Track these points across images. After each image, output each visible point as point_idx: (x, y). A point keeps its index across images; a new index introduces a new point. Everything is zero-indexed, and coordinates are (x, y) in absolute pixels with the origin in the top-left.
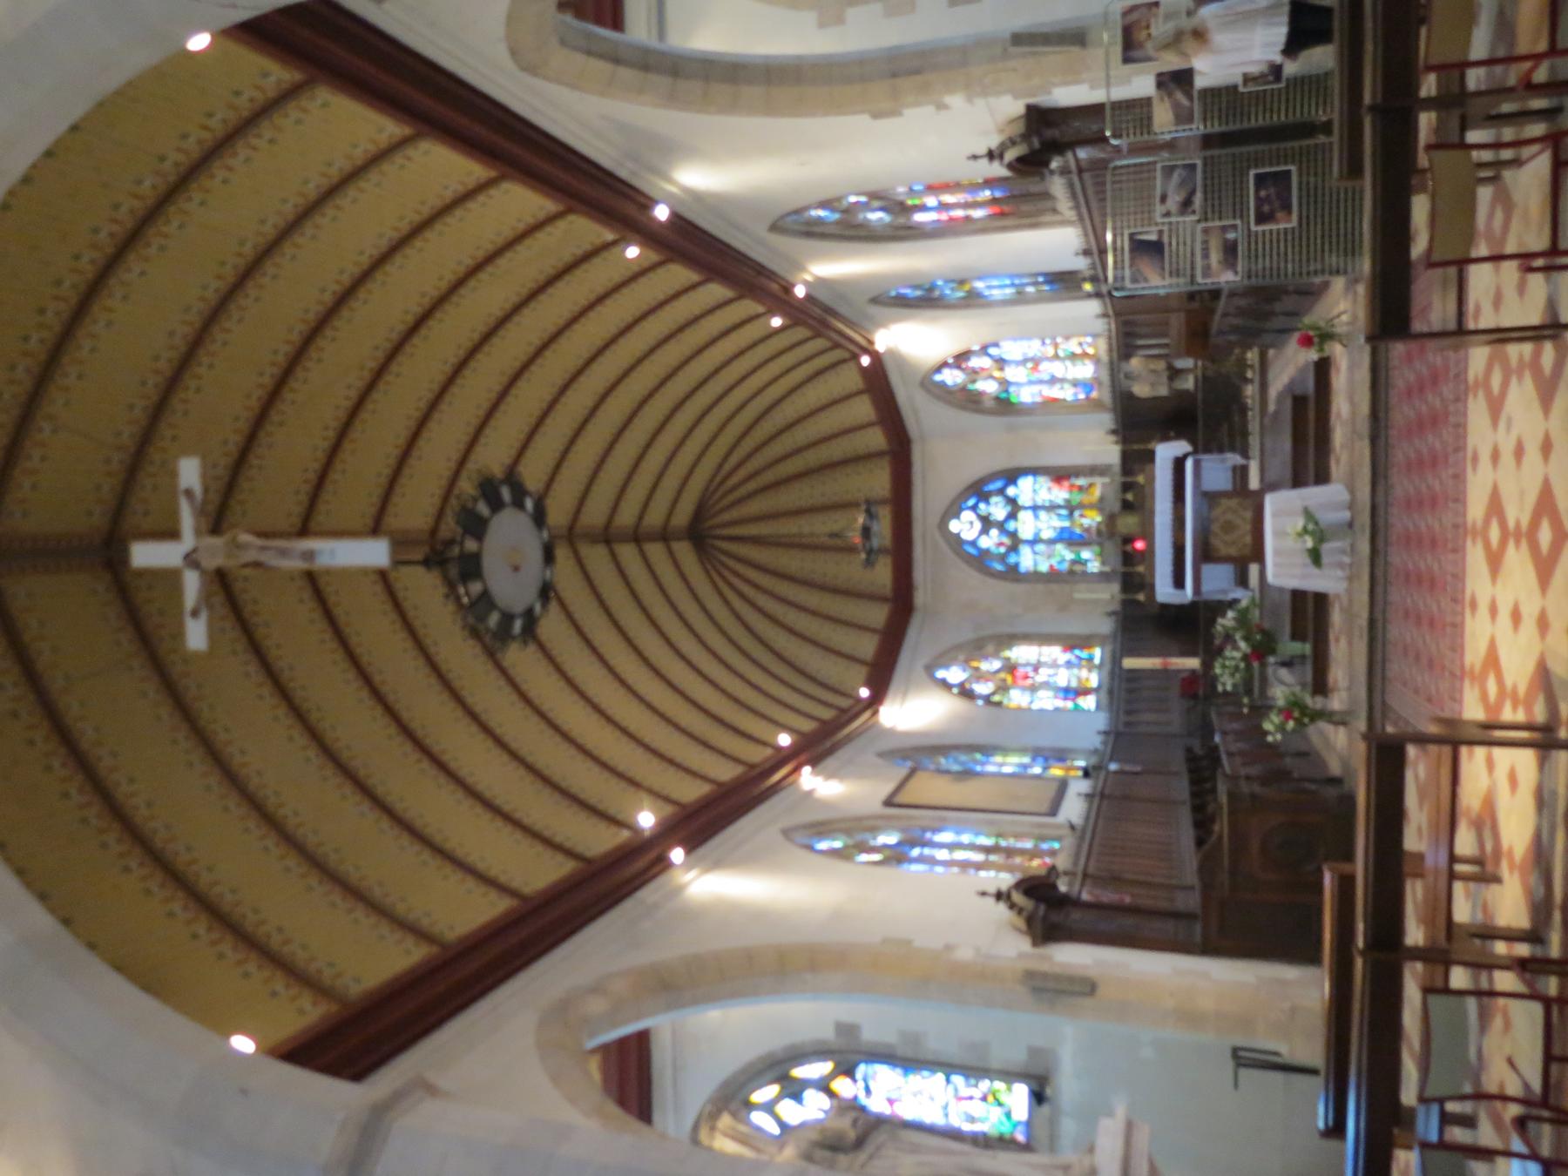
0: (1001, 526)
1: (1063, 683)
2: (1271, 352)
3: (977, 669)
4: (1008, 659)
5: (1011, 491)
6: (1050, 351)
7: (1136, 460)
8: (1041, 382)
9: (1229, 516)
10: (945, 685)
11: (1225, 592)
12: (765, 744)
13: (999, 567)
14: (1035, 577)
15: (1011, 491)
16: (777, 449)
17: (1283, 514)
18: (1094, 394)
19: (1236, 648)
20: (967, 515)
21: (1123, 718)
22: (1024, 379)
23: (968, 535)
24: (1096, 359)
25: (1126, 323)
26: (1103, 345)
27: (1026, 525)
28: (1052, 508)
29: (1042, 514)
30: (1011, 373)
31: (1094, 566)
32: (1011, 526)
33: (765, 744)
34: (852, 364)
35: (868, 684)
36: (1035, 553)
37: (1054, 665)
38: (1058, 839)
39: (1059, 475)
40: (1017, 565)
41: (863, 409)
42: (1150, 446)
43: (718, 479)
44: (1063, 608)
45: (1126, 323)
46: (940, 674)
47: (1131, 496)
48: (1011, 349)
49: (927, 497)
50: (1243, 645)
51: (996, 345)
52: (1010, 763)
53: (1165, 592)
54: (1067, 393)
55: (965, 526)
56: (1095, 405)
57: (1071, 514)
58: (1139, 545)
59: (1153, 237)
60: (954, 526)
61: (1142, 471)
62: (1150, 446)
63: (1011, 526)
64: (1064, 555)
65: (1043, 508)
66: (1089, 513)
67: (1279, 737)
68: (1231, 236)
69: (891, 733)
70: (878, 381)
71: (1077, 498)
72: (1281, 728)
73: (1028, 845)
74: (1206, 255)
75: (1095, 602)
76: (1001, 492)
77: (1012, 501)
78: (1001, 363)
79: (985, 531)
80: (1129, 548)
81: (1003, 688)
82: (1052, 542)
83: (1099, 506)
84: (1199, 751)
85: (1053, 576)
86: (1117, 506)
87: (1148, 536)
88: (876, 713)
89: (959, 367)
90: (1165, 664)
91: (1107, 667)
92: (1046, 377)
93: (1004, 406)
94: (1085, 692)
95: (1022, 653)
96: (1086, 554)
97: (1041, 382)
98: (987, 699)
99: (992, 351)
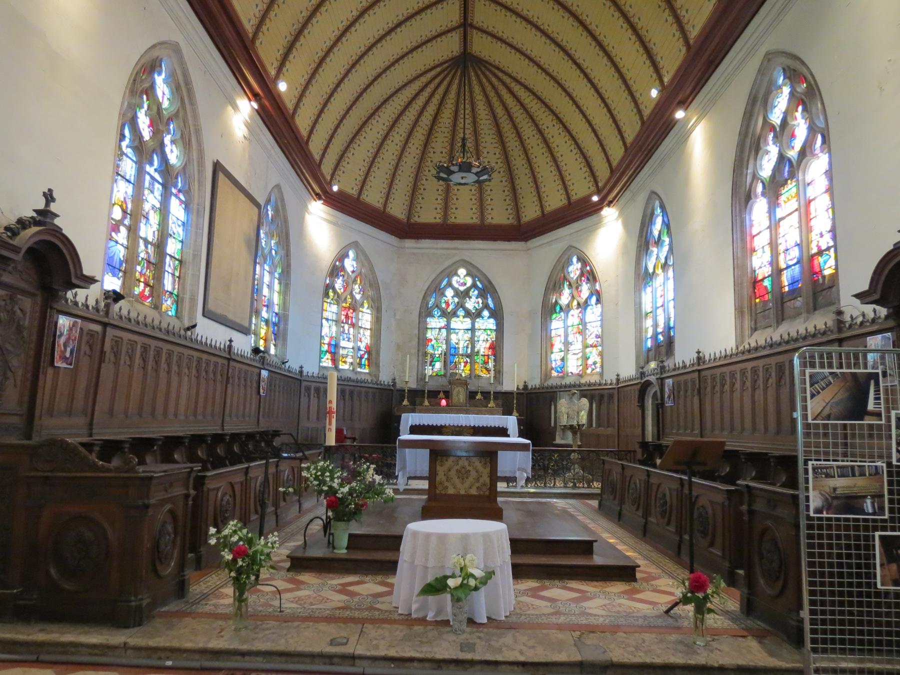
0: (460, 305)
1: (343, 343)
2: (595, 503)
3: (355, 281)
4: (362, 305)
5: (486, 313)
6: (591, 340)
7: (506, 402)
8: (566, 335)
9: (473, 474)
10: (342, 256)
11: (404, 468)
12: (279, 70)
13: (431, 302)
14: (423, 328)
15: (486, 313)
16: (528, 131)
17: (477, 542)
18: (554, 374)
19: (344, 482)
20: (469, 281)
21: (313, 385)
22: (569, 323)
23: (454, 280)
24: (580, 376)
25: (611, 396)
26: (595, 379)
27: (460, 323)
28: (472, 341)
29: (468, 335)
30: (575, 312)
31: (429, 371)
32: (461, 313)
33: (279, 70)
34: (593, 189)
35: (340, 192)
36: (440, 329)
37: (357, 339)
38: (178, 316)
39: (496, 348)
40: (433, 316)
41: (555, 201)
42: (515, 413)
43: (508, 80)
44: (399, 347)
45: (611, 396)
46: (351, 254)
47: (478, 399)
48: (594, 313)
49: (485, 253)
50: (346, 489)
51: (598, 301)
52: (271, 291)
53: (409, 419)
54: (556, 356)
55: (462, 278)
56: (547, 376)
57: (468, 356)
58: (444, 402)
59: (871, 406)
60: (462, 272)
61: (497, 405)
62: (515, 413)
63: (461, 313)
64: (438, 348)
65: (473, 335)
66: (468, 367)
67: (213, 541)
68: (868, 505)
69: (304, 208)
70: (580, 211)
71: (479, 359)
72: (225, 543)
73: (168, 283)
74: (844, 472)
75: (404, 372)
76: (486, 306)
77: (478, 314)
78: (584, 306)
79: (457, 293)
80: (442, 395)
81: (338, 299)
82: (448, 340)
83: (472, 375)
84: (277, 442)
85: (423, 342)
86: (472, 388)
87: (451, 408)
88: (319, 197)
89: (582, 274)
90: (330, 412)
91: (354, 377)
92: (570, 339)
93: (549, 310)
94: (334, 360)
95: (366, 318)
96: (438, 365)
97: (566, 335)
98: (329, 287)
99: (594, 299)
